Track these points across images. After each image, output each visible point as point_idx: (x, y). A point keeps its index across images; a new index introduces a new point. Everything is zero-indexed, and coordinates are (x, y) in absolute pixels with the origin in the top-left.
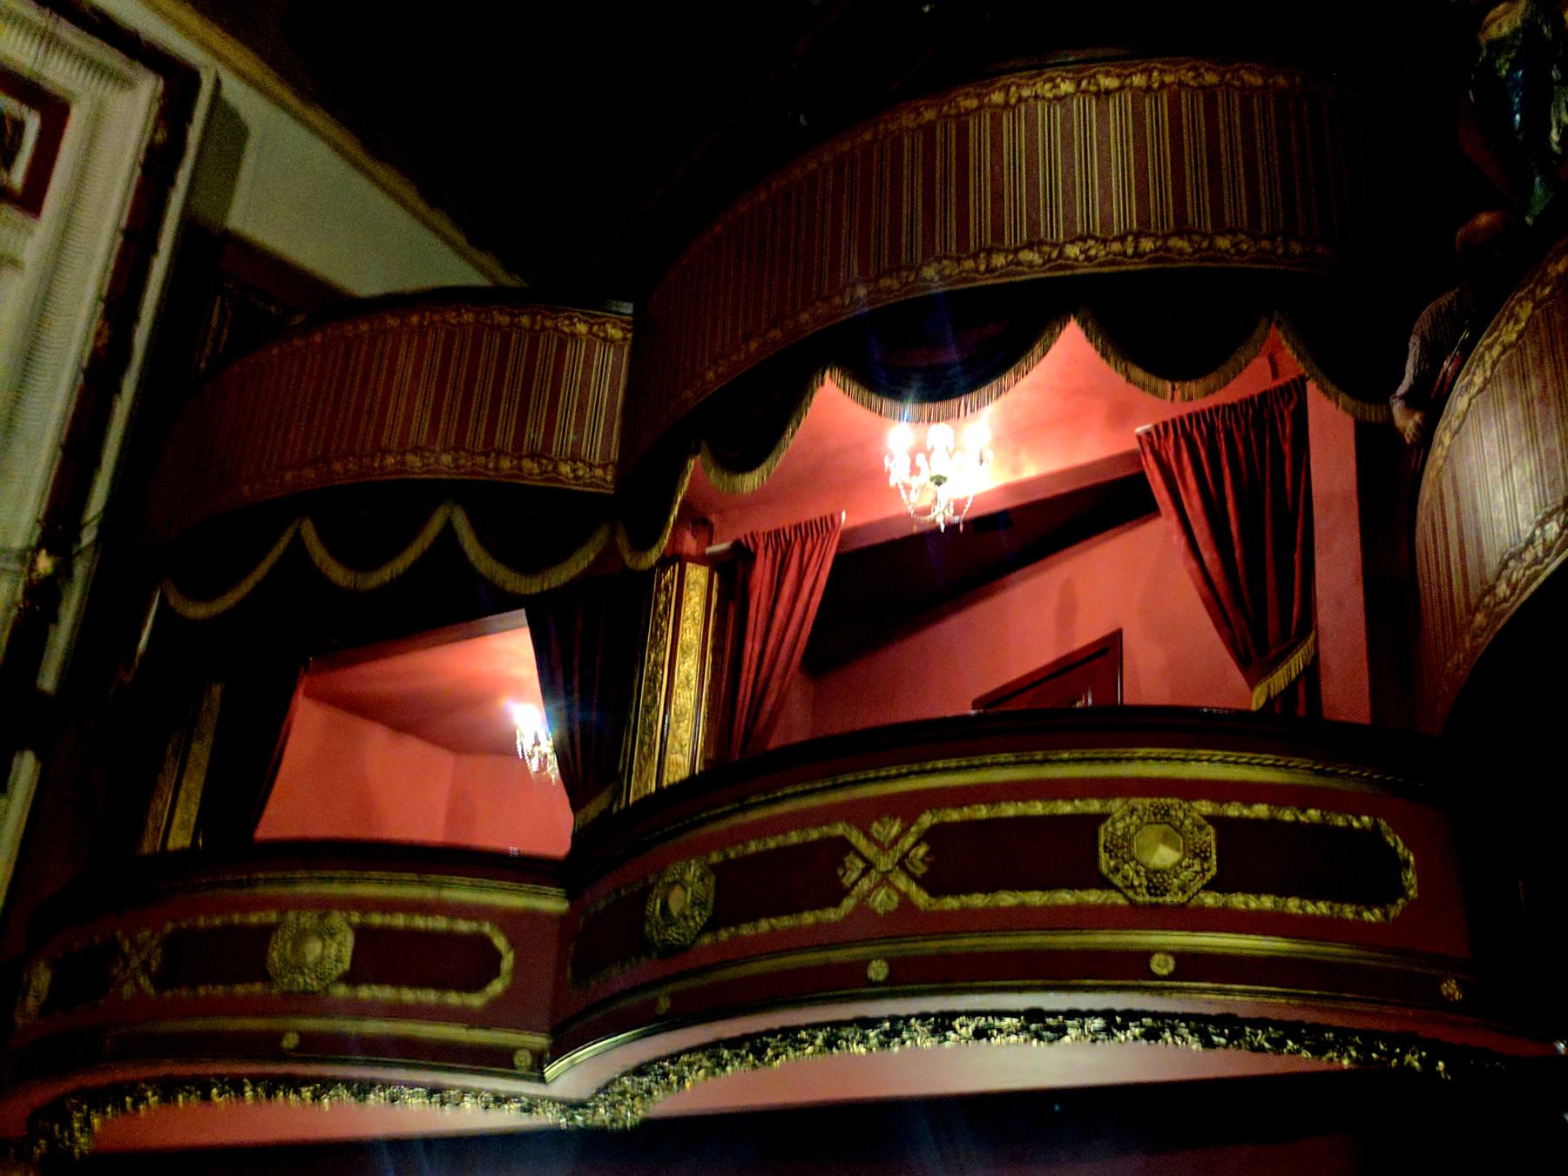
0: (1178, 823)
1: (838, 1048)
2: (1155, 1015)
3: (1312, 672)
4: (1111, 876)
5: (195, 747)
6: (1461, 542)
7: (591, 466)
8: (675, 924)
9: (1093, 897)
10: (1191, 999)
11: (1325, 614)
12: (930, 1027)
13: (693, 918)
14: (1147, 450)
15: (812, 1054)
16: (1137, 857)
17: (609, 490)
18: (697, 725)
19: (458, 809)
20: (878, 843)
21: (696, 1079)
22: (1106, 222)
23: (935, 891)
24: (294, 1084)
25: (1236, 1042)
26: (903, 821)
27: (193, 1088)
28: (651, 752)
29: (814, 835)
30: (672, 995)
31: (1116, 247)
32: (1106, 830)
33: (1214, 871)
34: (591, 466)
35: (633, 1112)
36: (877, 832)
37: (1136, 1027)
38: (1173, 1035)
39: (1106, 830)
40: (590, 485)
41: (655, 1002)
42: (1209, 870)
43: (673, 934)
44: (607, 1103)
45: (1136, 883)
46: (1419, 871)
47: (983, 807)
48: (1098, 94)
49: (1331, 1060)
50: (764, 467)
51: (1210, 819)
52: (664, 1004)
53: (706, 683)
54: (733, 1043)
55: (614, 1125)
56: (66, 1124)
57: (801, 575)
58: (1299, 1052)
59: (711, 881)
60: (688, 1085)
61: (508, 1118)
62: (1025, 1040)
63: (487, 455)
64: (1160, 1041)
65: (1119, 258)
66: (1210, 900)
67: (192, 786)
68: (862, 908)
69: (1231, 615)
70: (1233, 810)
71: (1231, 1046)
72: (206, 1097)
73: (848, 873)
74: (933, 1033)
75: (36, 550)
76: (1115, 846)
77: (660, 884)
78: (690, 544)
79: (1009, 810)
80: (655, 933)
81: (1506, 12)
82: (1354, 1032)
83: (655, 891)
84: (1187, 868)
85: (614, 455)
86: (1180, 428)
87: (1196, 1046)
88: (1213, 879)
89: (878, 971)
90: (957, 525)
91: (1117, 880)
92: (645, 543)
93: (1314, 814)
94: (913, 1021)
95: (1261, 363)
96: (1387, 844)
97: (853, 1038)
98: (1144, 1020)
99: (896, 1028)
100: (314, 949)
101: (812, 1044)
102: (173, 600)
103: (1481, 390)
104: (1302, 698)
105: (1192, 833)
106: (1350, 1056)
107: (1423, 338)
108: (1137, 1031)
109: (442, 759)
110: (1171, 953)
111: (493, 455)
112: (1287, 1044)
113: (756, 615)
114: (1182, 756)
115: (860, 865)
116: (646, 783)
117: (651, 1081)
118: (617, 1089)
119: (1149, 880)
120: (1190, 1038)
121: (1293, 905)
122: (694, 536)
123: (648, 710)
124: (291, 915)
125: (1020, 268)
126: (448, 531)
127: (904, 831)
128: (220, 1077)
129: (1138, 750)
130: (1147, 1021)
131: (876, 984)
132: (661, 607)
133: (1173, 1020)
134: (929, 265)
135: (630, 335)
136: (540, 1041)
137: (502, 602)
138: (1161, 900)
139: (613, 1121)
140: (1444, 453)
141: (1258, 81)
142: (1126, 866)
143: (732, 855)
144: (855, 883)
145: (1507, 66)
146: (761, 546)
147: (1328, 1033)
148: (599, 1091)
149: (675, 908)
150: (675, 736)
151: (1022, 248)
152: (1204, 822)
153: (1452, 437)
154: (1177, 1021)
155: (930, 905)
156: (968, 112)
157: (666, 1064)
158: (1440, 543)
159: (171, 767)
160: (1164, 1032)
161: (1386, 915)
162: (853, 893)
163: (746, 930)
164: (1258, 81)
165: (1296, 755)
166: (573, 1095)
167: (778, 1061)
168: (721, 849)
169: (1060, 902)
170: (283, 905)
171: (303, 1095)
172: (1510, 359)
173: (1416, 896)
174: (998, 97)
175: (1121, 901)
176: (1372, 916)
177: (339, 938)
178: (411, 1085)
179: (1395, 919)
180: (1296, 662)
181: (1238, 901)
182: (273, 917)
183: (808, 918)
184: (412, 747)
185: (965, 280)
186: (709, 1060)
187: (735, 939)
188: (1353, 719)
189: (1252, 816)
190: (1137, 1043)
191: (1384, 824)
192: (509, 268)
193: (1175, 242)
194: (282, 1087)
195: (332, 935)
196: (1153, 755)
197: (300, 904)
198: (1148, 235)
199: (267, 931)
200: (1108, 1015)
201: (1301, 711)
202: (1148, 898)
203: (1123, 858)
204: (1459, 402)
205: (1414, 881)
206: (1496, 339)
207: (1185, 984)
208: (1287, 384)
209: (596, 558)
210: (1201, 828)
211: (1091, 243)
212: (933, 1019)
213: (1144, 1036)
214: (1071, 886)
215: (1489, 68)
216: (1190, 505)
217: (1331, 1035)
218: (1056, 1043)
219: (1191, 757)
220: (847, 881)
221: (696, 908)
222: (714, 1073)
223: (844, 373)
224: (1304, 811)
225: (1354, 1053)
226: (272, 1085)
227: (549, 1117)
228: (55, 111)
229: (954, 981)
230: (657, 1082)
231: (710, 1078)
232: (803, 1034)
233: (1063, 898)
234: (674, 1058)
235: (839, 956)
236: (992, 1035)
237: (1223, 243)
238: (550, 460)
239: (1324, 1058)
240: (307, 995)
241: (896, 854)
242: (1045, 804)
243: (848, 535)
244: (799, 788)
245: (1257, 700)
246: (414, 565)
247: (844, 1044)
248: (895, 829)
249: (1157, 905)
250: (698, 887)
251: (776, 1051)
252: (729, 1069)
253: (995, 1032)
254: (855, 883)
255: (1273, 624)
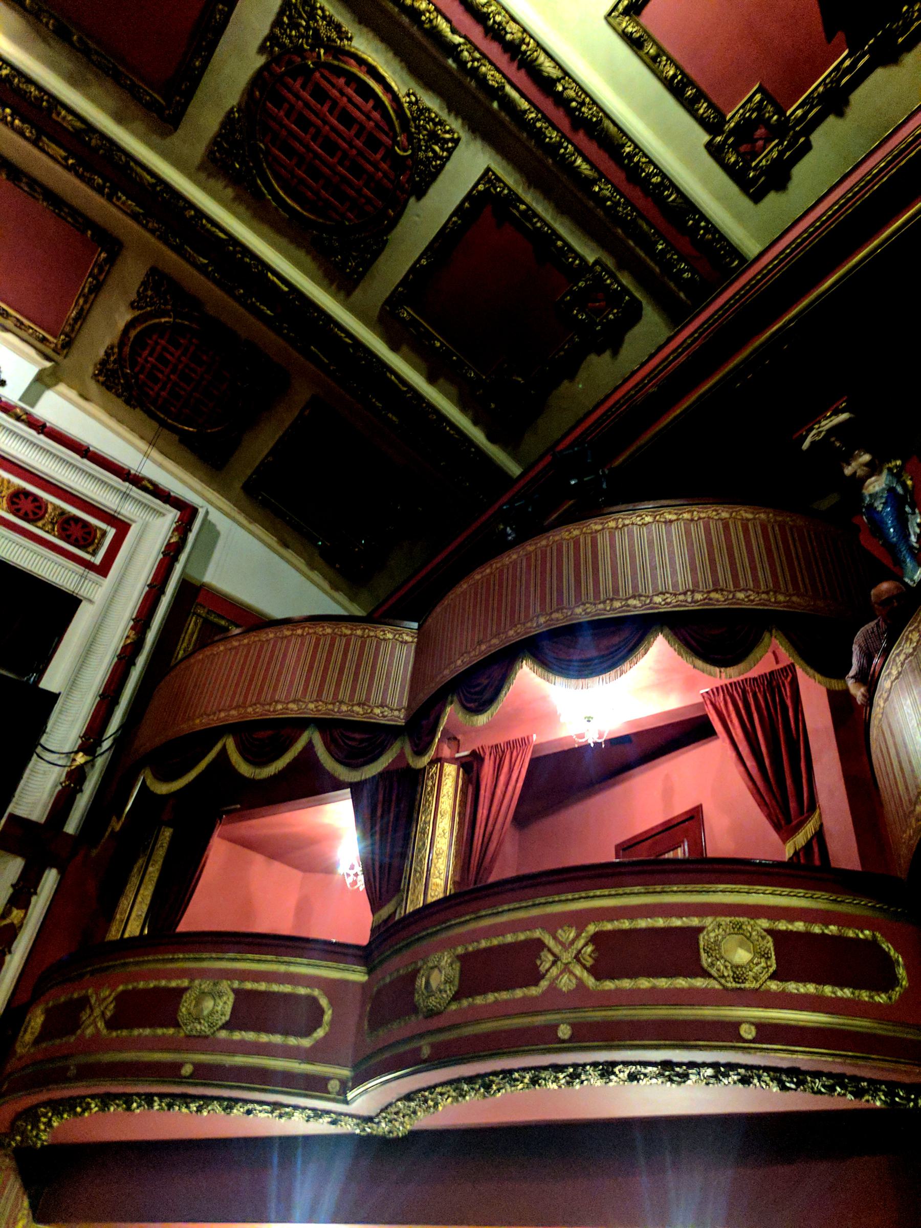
0: (748, 934)
1: (539, 1085)
2: (747, 1067)
3: (820, 835)
4: (709, 969)
5: (150, 869)
6: (900, 762)
7: (392, 710)
8: (433, 995)
9: (699, 983)
10: (769, 1057)
11: (823, 798)
12: (599, 1072)
13: (446, 992)
14: (708, 702)
15: (522, 1089)
16: (725, 956)
17: (402, 723)
18: (449, 861)
19: (303, 909)
20: (562, 944)
21: (445, 1104)
22: (675, 585)
23: (598, 978)
24: (186, 1099)
25: (802, 1087)
26: (577, 928)
27: (121, 1102)
28: (421, 877)
29: (522, 937)
30: (432, 1046)
31: (681, 597)
32: (704, 938)
33: (774, 967)
34: (392, 710)
35: (404, 1127)
36: (561, 935)
37: (734, 1075)
38: (759, 1081)
39: (704, 938)
40: (392, 720)
41: (419, 1049)
42: (771, 966)
43: (433, 1002)
44: (387, 1120)
45: (726, 974)
46: (907, 968)
47: (626, 921)
48: (665, 522)
49: (868, 1101)
50: (489, 712)
51: (769, 932)
52: (426, 1052)
53: (455, 834)
54: (470, 1080)
55: (391, 1135)
56: (35, 1126)
57: (511, 770)
58: (844, 1095)
59: (457, 966)
60: (440, 1108)
61: (321, 1127)
62: (662, 1082)
63: (334, 704)
64: (751, 1085)
65: (684, 603)
66: (774, 986)
67: (146, 893)
68: (553, 988)
69: (767, 798)
70: (782, 926)
71: (799, 1089)
72: (129, 1108)
73: (544, 963)
74: (602, 1076)
75: (76, 752)
76: (710, 949)
77: (425, 967)
78: (446, 752)
79: (642, 923)
80: (421, 1001)
81: (876, 481)
82: (882, 1082)
83: (422, 972)
84: (757, 964)
85: (405, 703)
86: (726, 690)
87: (775, 1089)
88: (775, 972)
89: (564, 1032)
90: (601, 743)
91: (713, 972)
92: (420, 751)
93: (833, 929)
94: (588, 1067)
95: (769, 655)
96: (883, 950)
97: (549, 1078)
98: (739, 1070)
99: (576, 1073)
100: (208, 1004)
101: (522, 1082)
102: (148, 782)
103: (897, 678)
104: (816, 850)
105: (758, 941)
106: (880, 1099)
107: (860, 646)
108: (736, 1078)
109: (297, 875)
110: (752, 1024)
111: (337, 704)
112: (836, 1090)
113: (485, 794)
114: (746, 890)
115: (551, 958)
116: (418, 897)
117: (416, 1105)
118: (394, 1109)
119: (734, 973)
120: (771, 1084)
121: (828, 990)
122: (449, 748)
123: (420, 850)
124: (197, 982)
125: (629, 608)
126: (310, 746)
127: (578, 936)
128: (139, 1095)
129: (719, 886)
130: (742, 1071)
131: (564, 1041)
132: (429, 789)
133: (759, 1070)
134: (578, 606)
135: (416, 640)
136: (346, 1073)
137: (338, 785)
138: (743, 986)
139: (390, 1132)
140: (881, 711)
141: (750, 516)
142: (718, 963)
143: (470, 949)
144: (547, 971)
145: (882, 505)
146: (488, 753)
147: (864, 1082)
148: (382, 1111)
149: (434, 984)
150: (436, 867)
151: (630, 598)
152: (764, 934)
153: (885, 703)
154: (761, 1071)
155: (596, 986)
156: (597, 531)
157: (427, 1094)
158: (887, 761)
159: (134, 880)
160: (753, 1079)
161: (890, 998)
162: (548, 976)
163: (479, 1000)
164: (750, 516)
165: (820, 890)
166: (365, 1113)
167: (500, 1094)
168: (463, 945)
169: (678, 986)
170: (191, 974)
171: (191, 1109)
172: (911, 661)
173: (907, 985)
174: (612, 524)
175: (718, 986)
176: (881, 998)
177: (225, 998)
178: (261, 1103)
179: (896, 1001)
180: (809, 829)
181: (792, 987)
182: (185, 983)
183: (519, 993)
184: (277, 866)
185: (599, 615)
186: (454, 1091)
187: (471, 1006)
188: (849, 867)
189: (795, 929)
190: (736, 1086)
191: (879, 936)
192: (352, 599)
193: (713, 595)
194: (178, 1103)
195: (220, 997)
196: (729, 890)
197: (203, 974)
198: (699, 592)
199: (181, 991)
200: (715, 1065)
201: (817, 862)
202: (734, 985)
203: (716, 957)
204: (885, 684)
205: (904, 974)
206: (901, 651)
207: (765, 1046)
208: (785, 668)
209: (393, 761)
210: (763, 938)
211: (668, 595)
212: (601, 1067)
213: (740, 1081)
214: (686, 976)
215: (871, 507)
216: (736, 734)
217: (865, 1084)
218: (683, 1085)
219: (752, 891)
220: (542, 969)
221: (447, 985)
222: (458, 1101)
223: (533, 662)
224: (827, 927)
225: (883, 1098)
226: (173, 1100)
227: (348, 1127)
228: (122, 527)
229: (613, 1040)
230: (420, 1106)
231: (455, 1104)
232: (516, 1075)
233: (681, 984)
234: (431, 1088)
235: (539, 1020)
236: (640, 1079)
237: (741, 595)
238: (369, 706)
239: (863, 1100)
240: (203, 1037)
241: (573, 951)
242: (665, 920)
243: (537, 747)
244: (512, 906)
245: (788, 851)
246: (289, 764)
247: (543, 1082)
248: (572, 935)
249: (740, 989)
250: (448, 970)
251: (498, 1086)
252: (467, 1098)
253: (642, 1077)
254: (547, 971)
255: (792, 805)
